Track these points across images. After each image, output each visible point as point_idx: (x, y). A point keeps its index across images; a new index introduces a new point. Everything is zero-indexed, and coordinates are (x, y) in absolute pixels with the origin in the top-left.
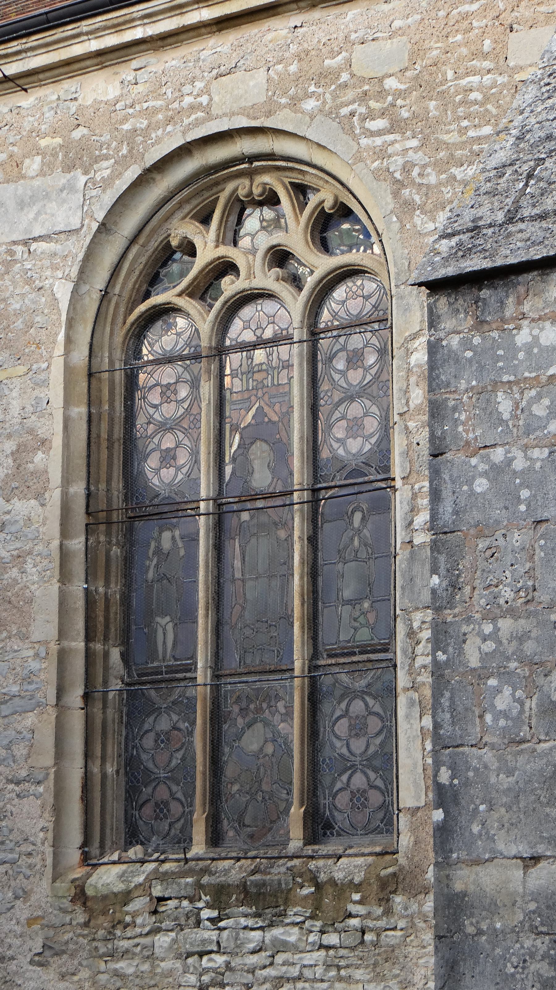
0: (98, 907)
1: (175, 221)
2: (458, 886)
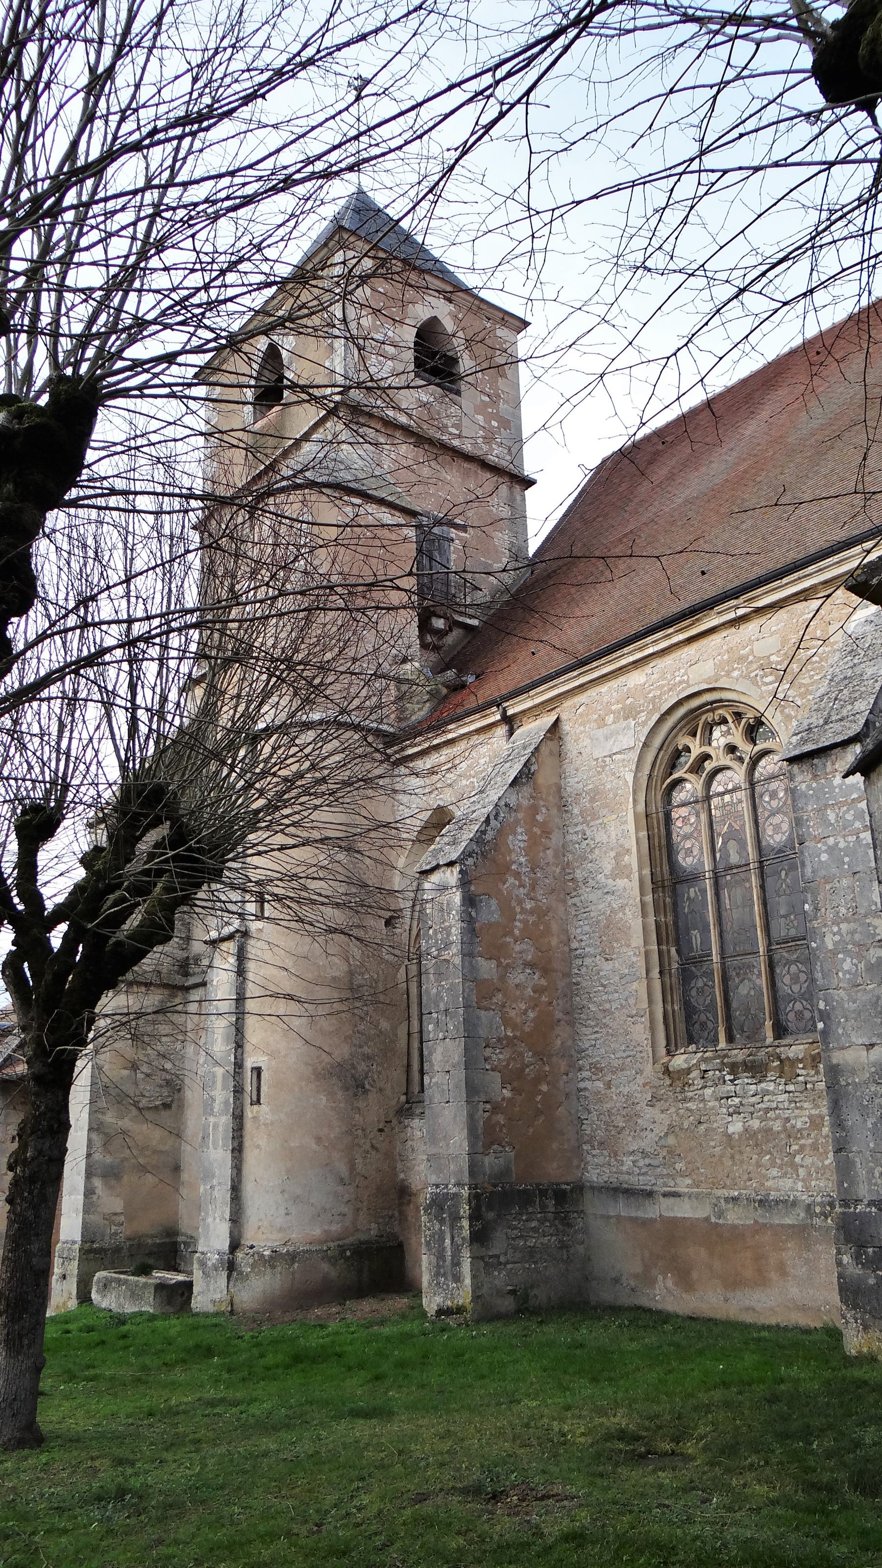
0: (676, 1076)
1: (680, 737)
2: (835, 1061)
